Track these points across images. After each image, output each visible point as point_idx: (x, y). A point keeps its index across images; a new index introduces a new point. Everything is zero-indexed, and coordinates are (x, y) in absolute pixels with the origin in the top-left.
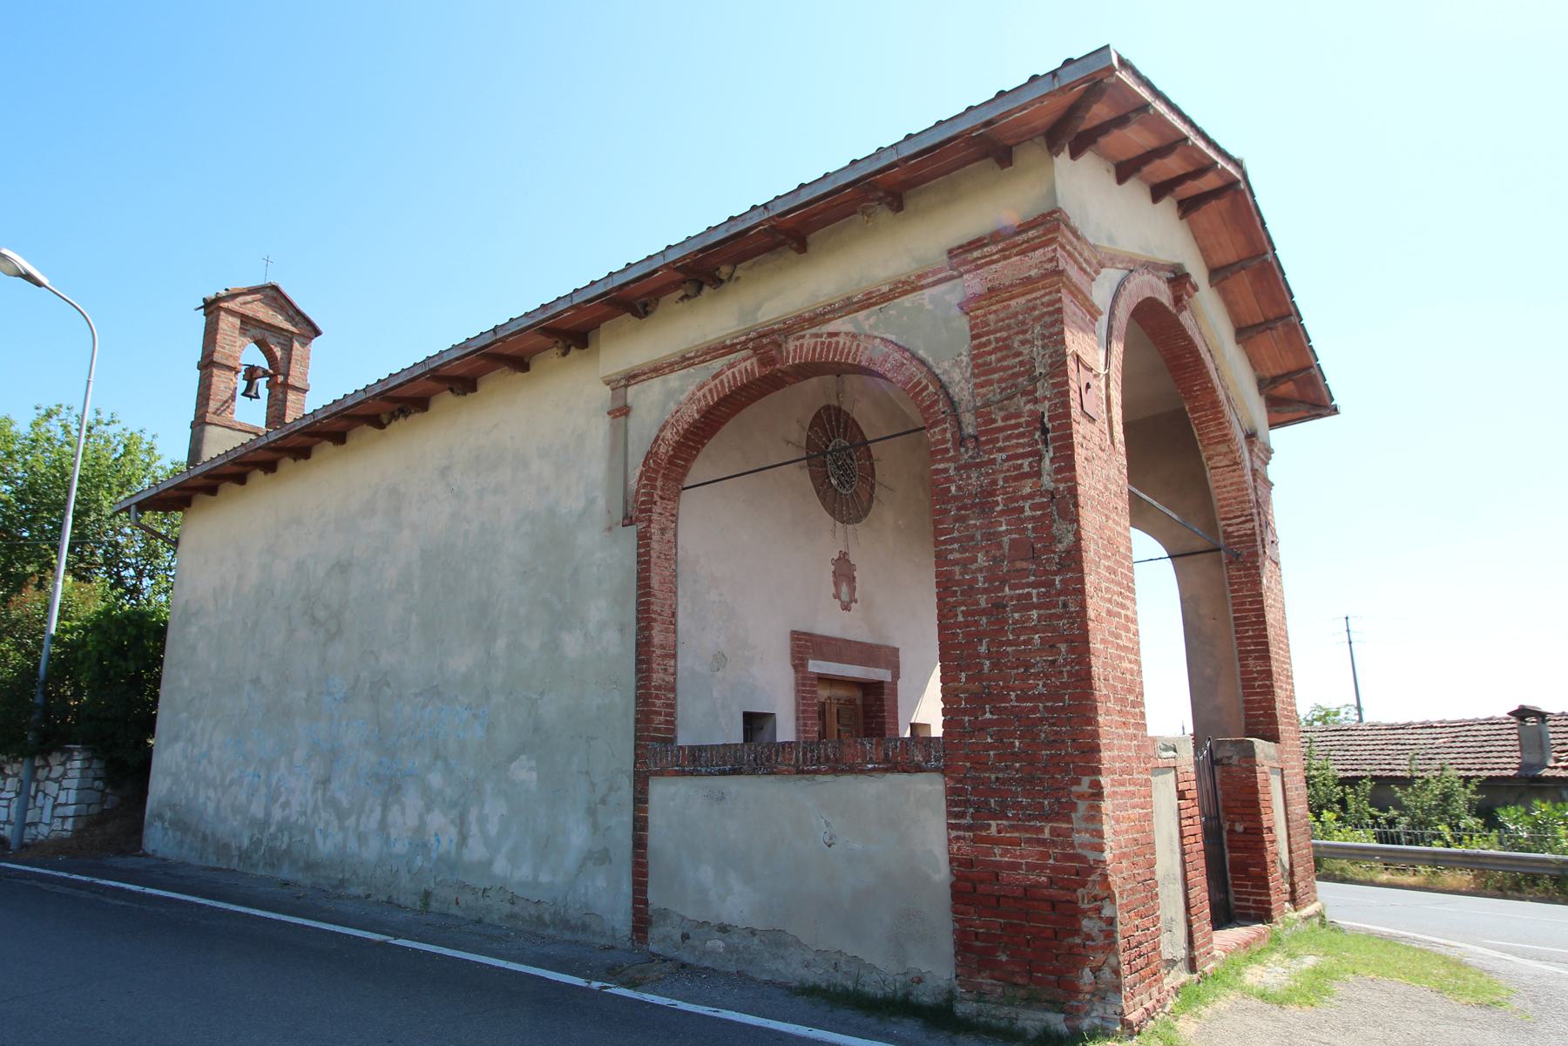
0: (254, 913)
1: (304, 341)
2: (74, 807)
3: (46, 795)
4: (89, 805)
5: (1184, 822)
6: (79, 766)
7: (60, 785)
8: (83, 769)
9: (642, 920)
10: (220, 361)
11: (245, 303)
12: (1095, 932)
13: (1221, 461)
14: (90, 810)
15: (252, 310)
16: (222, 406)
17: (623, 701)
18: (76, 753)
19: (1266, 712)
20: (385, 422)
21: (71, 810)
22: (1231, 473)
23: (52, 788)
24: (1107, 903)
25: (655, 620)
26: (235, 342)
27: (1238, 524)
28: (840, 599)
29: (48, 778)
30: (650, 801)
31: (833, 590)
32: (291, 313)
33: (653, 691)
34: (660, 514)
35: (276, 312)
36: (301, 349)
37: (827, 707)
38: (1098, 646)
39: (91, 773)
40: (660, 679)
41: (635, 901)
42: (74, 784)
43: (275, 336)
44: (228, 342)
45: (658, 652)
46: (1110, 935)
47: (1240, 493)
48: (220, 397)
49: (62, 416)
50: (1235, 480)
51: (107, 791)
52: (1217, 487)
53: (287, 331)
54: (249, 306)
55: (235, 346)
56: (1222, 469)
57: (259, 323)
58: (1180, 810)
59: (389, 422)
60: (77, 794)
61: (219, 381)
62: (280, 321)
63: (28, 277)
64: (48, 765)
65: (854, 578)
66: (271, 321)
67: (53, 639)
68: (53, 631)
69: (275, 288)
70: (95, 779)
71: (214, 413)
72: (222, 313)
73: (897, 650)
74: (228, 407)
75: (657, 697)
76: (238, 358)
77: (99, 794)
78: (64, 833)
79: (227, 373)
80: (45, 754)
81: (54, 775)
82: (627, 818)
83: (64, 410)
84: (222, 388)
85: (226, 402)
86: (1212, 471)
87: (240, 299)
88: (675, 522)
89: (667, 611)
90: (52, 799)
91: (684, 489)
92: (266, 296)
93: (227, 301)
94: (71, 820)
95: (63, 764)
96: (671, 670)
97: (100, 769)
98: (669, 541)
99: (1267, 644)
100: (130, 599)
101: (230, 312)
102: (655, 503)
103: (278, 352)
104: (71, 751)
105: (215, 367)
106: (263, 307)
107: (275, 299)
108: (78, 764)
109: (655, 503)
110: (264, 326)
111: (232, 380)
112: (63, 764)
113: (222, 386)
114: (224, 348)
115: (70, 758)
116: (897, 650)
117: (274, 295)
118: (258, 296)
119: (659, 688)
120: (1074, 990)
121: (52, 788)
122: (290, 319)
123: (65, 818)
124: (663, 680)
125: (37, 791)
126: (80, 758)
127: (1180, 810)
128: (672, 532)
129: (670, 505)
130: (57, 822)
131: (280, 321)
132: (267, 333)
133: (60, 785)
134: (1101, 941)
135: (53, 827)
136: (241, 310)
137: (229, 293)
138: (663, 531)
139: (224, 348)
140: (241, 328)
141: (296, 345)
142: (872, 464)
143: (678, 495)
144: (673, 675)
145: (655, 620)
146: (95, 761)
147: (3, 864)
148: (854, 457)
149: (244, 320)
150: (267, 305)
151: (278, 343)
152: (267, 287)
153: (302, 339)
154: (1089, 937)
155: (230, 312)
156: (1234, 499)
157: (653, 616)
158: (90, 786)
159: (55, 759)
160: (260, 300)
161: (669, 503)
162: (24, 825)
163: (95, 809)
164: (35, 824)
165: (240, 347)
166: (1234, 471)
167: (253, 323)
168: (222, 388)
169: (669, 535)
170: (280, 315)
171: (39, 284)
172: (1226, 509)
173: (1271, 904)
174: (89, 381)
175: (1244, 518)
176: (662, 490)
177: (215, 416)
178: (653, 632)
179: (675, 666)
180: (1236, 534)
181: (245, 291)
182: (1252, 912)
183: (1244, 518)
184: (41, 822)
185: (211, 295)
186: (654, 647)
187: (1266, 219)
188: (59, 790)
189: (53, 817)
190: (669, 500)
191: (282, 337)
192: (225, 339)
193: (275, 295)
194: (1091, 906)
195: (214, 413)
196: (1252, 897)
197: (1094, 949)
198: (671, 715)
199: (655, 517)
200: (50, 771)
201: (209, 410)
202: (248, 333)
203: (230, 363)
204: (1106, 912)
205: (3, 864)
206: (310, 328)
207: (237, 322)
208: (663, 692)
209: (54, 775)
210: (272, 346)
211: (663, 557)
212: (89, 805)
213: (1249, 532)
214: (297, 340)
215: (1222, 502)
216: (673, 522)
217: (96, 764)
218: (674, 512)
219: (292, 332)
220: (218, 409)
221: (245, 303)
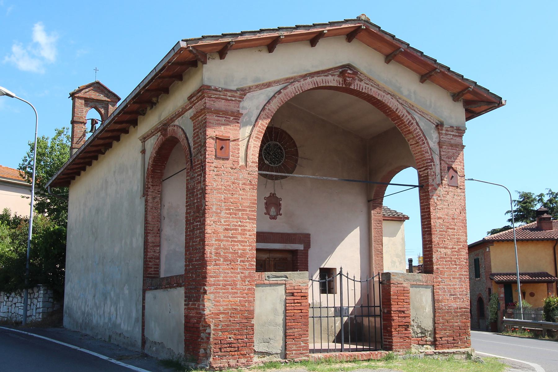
0: (75, 347)
1: (114, 104)
2: (42, 309)
3: (34, 304)
4: (48, 308)
5: (287, 305)
6: (42, 292)
7: (38, 300)
8: (44, 294)
9: (144, 341)
10: (77, 120)
11: (86, 93)
12: (204, 337)
13: (412, 141)
14: (48, 310)
15: (90, 95)
16: (79, 140)
17: (139, 263)
18: (41, 288)
19: (430, 260)
20: (103, 152)
21: (41, 310)
22: (417, 147)
23: (35, 301)
24: (208, 328)
25: (150, 233)
26: (83, 111)
27: (423, 171)
28: (269, 214)
29: (34, 298)
30: (146, 300)
32: (106, 92)
33: (148, 259)
34: (153, 192)
35: (100, 93)
36: (113, 108)
37: (267, 262)
38: (117, 250)
39: (47, 295)
40: (151, 255)
41: (142, 336)
42: (41, 300)
43: (101, 104)
44: (80, 111)
45: (151, 245)
46: (208, 338)
47: (422, 156)
48: (78, 136)
49: (65, 133)
50: (419, 150)
51: (55, 303)
52: (414, 154)
53: (105, 101)
54: (88, 93)
55: (83, 112)
56: (414, 145)
57: (92, 100)
58: (286, 300)
59: (105, 152)
60: (43, 304)
61: (77, 129)
62: (102, 97)
63: (7, 95)
64: (33, 292)
65: (280, 205)
66: (98, 98)
67: (31, 242)
68: (31, 239)
69: (98, 83)
70: (49, 298)
71: (76, 143)
72: (76, 99)
73: (309, 235)
74: (82, 140)
75: (150, 261)
76: (85, 117)
77: (52, 304)
78: (39, 319)
79: (80, 125)
80: (32, 287)
81: (36, 296)
82: (141, 306)
83: (65, 130)
84: (79, 132)
85: (81, 137)
86: (411, 146)
87: (83, 91)
88: (161, 194)
89: (156, 229)
90: (35, 306)
91: (163, 181)
92: (94, 87)
93: (78, 94)
94: (41, 314)
95: (38, 292)
96: (158, 251)
97: (51, 294)
98: (157, 202)
99: (430, 227)
100: (57, 222)
101: (79, 98)
102: (149, 188)
103: (103, 111)
104: (39, 287)
105: (75, 123)
106: (93, 93)
107: (99, 88)
108: (42, 292)
109: (149, 188)
110: (95, 101)
111: (82, 127)
112: (38, 292)
113: (79, 131)
114: (78, 114)
115: (39, 290)
116: (309, 235)
117: (98, 86)
118: (91, 88)
119: (152, 258)
120: (197, 354)
121: (35, 301)
122: (106, 96)
123: (39, 313)
124: (154, 255)
125: (31, 303)
126: (43, 289)
127: (286, 300)
128: (159, 198)
129: (157, 188)
130: (37, 315)
131: (102, 97)
132: (97, 103)
133: (38, 300)
134: (205, 340)
135: (36, 317)
136: (84, 96)
137: (80, 89)
138: (154, 198)
139: (78, 114)
140: (85, 104)
141: (110, 106)
142: (297, 149)
143: (161, 183)
144: (158, 253)
145: (150, 233)
146: (49, 290)
147: (1, 327)
148: (283, 148)
149: (86, 100)
150: (95, 91)
151: (102, 107)
152: (95, 83)
153: (112, 103)
154: (202, 339)
155: (79, 98)
156: (421, 159)
157: (148, 231)
158: (48, 301)
159: (35, 290)
160: (92, 90)
161: (157, 187)
162: (26, 316)
163: (50, 310)
164: (31, 316)
165: (86, 112)
166: (418, 146)
167: (90, 100)
168: (79, 132)
169: (158, 199)
170: (102, 94)
171: (12, 97)
172: (419, 164)
173: (392, 343)
174: (36, 134)
175: (424, 168)
176: (152, 182)
177: (76, 145)
178: (148, 237)
179: (160, 249)
180: (422, 176)
181: (85, 87)
182: (388, 346)
183: (424, 168)
184: (33, 315)
185: (72, 91)
186: (148, 243)
187: (393, 33)
188: (37, 302)
189: (36, 313)
190: (156, 186)
191: (104, 104)
192: (78, 110)
193: (99, 86)
194: (203, 329)
195: (76, 143)
196: (388, 340)
197: (203, 343)
198: (157, 268)
199: (150, 193)
200: (34, 295)
201: (74, 142)
202: (88, 105)
203: (81, 120)
204: (207, 331)
205: (1, 327)
206: (115, 97)
207: (83, 102)
208: (153, 260)
209: (36, 296)
210: (100, 109)
211: (154, 208)
212: (48, 308)
213: (426, 174)
214: (110, 104)
215: (418, 161)
216: (159, 194)
217: (49, 292)
218: (159, 190)
219: (108, 101)
220: (77, 141)
221: (86, 93)
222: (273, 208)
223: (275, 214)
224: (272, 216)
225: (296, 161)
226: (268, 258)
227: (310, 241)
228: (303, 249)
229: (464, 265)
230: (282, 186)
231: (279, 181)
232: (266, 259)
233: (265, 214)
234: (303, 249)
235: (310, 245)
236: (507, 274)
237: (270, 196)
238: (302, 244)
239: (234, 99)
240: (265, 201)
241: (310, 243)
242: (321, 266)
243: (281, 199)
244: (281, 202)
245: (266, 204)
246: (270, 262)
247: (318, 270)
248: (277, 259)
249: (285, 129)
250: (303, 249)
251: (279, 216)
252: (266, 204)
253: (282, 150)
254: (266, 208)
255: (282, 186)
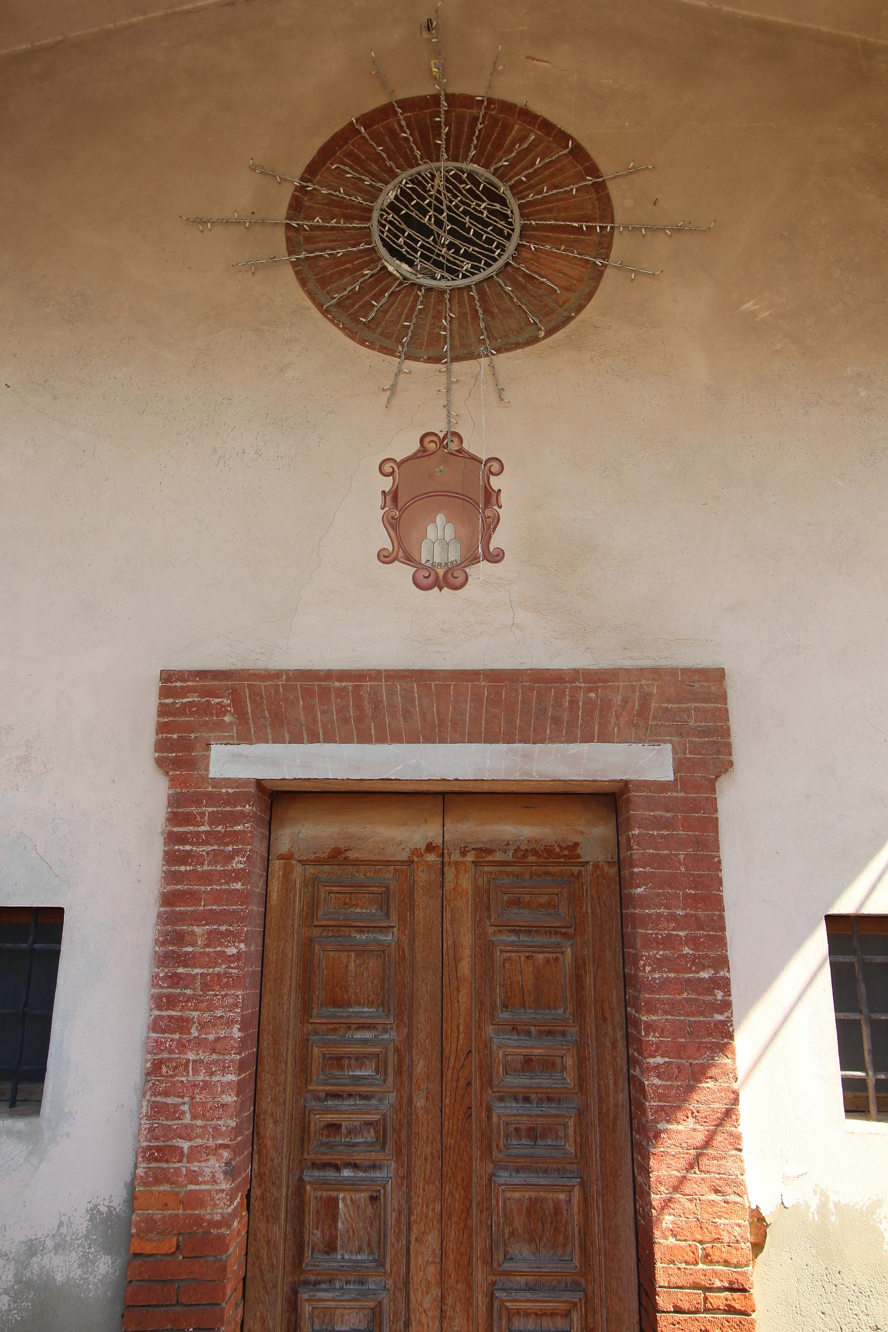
28: (409, 559)
31: (385, 541)
37: (421, 877)
65: (490, 497)
94: (577, 1187)
148: (503, 189)
222: (440, 518)
223: (454, 555)
224: (430, 569)
225: (604, 246)
226: (430, 848)
227: (724, 715)
228: (671, 777)
229: (84, 1273)
230: (500, 391)
231: (484, 361)
232: (415, 851)
233: (385, 558)
234: (667, 774)
235: (725, 748)
236: (446, 492)
237: (422, 452)
238: (658, 742)
239: (515, 300)
240: (387, 484)
241: (726, 732)
242: (836, 897)
243: (495, 467)
244: (495, 483)
245: (392, 497)
246: (450, 872)
247: (796, 944)
248: (498, 856)
249: (519, 99)
250: (671, 777)
251: (484, 565)
252: (395, 499)
253: (503, 201)
254: (393, 524)
255: (500, 391)
